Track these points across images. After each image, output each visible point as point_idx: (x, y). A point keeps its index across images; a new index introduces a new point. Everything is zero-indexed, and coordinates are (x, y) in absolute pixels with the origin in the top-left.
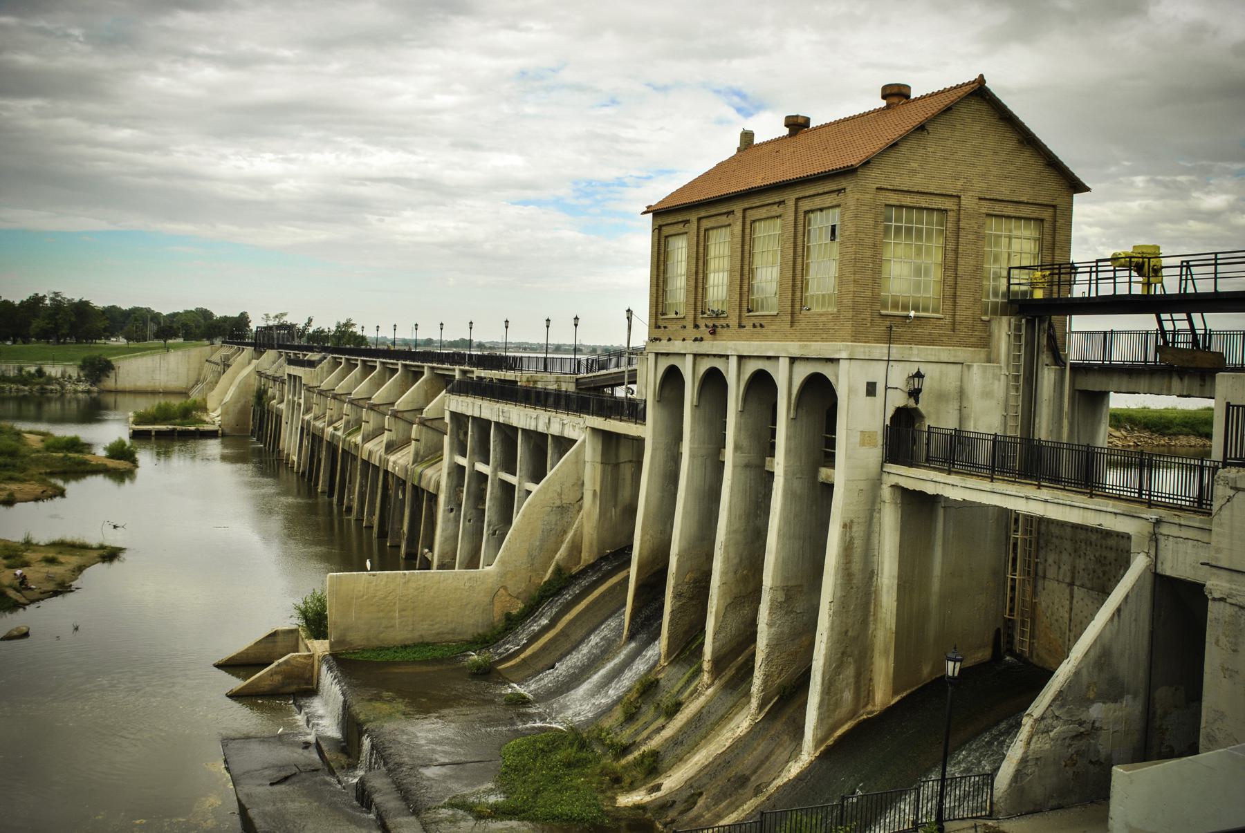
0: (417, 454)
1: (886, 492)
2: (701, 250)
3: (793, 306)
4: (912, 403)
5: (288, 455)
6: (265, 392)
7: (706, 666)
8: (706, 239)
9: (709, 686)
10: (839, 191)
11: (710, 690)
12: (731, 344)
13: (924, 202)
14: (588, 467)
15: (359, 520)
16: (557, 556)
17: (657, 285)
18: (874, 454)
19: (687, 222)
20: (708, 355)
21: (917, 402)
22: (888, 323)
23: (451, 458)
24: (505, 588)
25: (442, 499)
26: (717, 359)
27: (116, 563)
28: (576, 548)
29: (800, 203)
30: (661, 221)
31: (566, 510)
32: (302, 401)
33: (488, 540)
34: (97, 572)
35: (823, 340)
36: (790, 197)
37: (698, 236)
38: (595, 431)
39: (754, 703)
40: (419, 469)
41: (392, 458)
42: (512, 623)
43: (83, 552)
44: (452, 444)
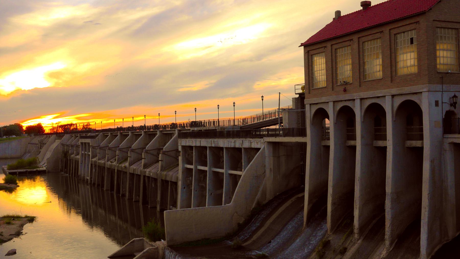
0: (162, 166)
1: (447, 147)
2: (334, 58)
3: (391, 74)
4: (452, 109)
5: (84, 177)
6: (67, 152)
7: (356, 231)
8: (336, 53)
9: (358, 240)
10: (417, 22)
11: (360, 241)
12: (355, 94)
13: (450, 25)
14: (267, 160)
15: (130, 199)
16: (257, 198)
17: (309, 75)
18: (440, 131)
19: (325, 47)
20: (341, 101)
21: (455, 107)
22: (441, 76)
23: (183, 166)
24: (237, 213)
25: (180, 183)
26: (347, 102)
27: (34, 222)
28: (264, 194)
29: (360, 39)
30: (308, 49)
31: (258, 177)
32: (90, 153)
33: (209, 198)
34: (27, 227)
35: (411, 85)
36: (386, 30)
37: (332, 52)
38: (269, 143)
39: (387, 243)
40: (165, 173)
41: (147, 170)
42: (241, 227)
43: (20, 219)
44: (183, 159)
